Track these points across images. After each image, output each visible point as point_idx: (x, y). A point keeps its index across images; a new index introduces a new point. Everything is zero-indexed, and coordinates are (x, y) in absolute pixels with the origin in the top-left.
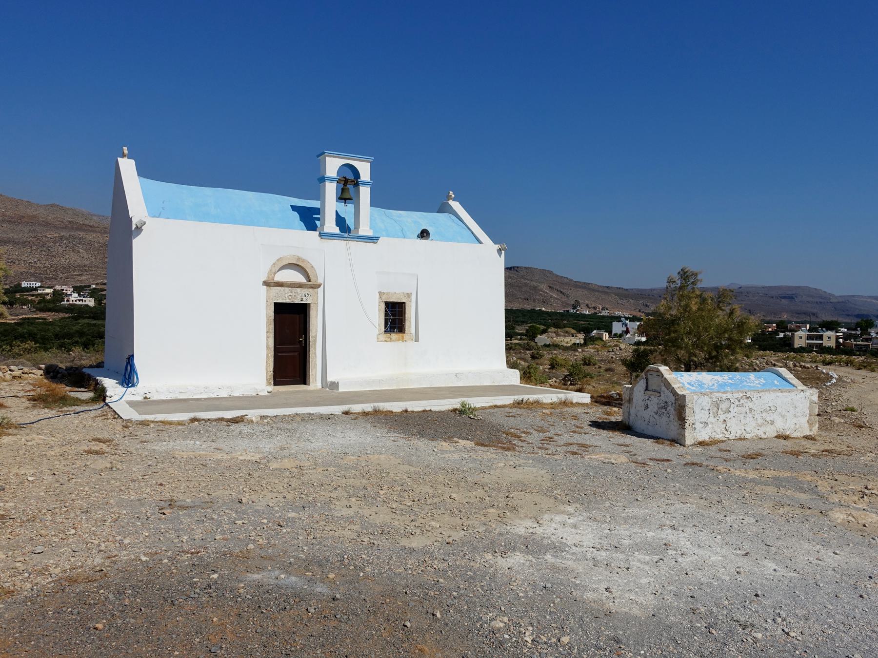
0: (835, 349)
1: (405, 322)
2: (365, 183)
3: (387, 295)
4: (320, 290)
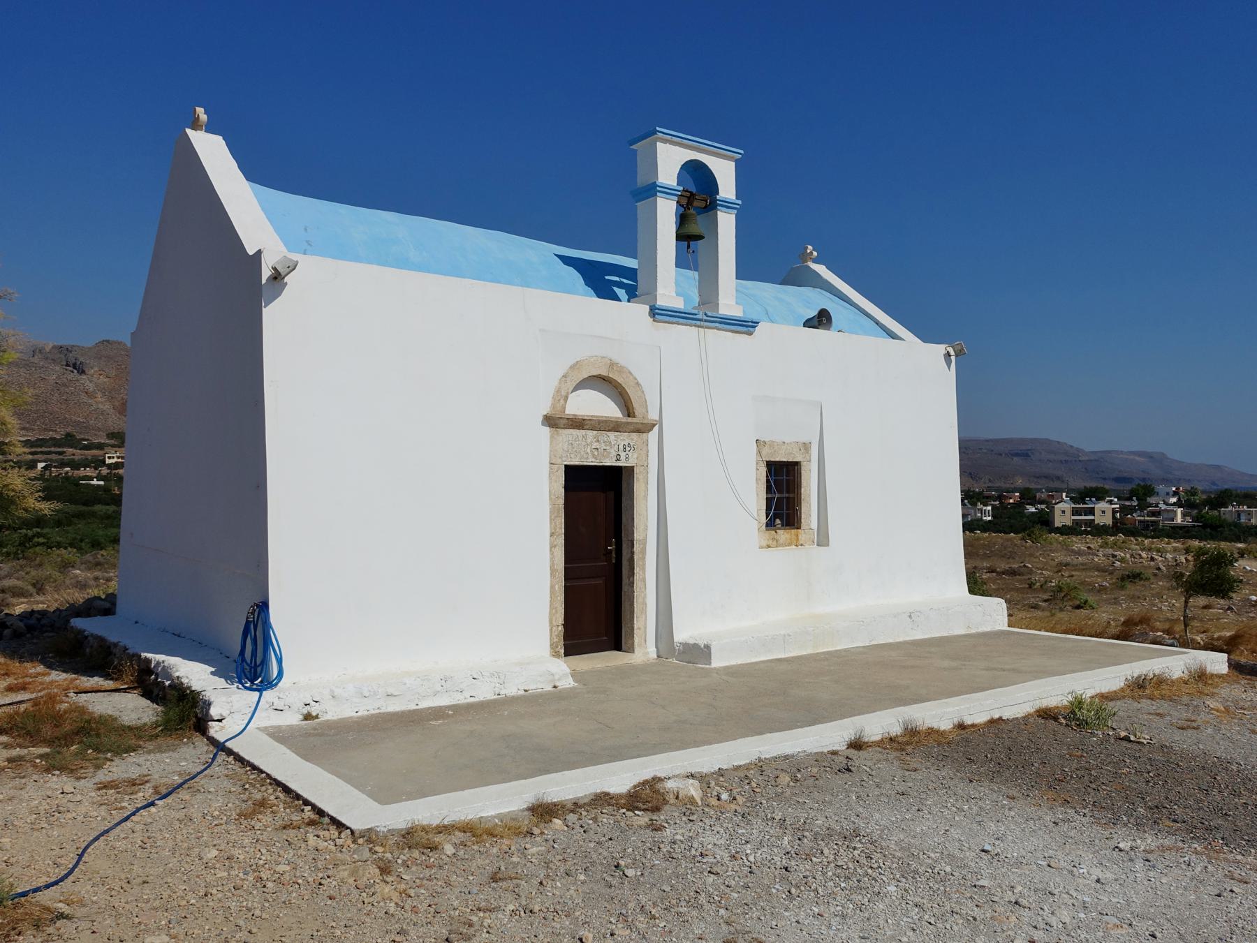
0: (1112, 527)
1: (799, 504)
2: (728, 205)
3: (770, 446)
4: (653, 436)
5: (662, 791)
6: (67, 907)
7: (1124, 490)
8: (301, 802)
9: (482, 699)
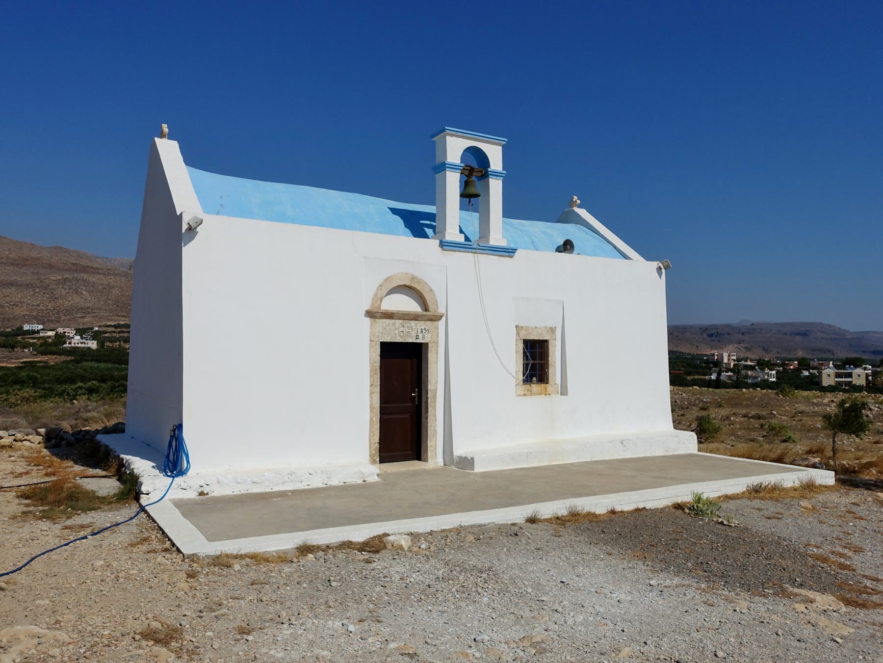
0: (866, 387)
1: (548, 368)
2: (496, 174)
3: (526, 330)
4: (442, 323)
5: (385, 541)
6: (5, 585)
7: (876, 360)
8: (167, 539)
9: (314, 487)
